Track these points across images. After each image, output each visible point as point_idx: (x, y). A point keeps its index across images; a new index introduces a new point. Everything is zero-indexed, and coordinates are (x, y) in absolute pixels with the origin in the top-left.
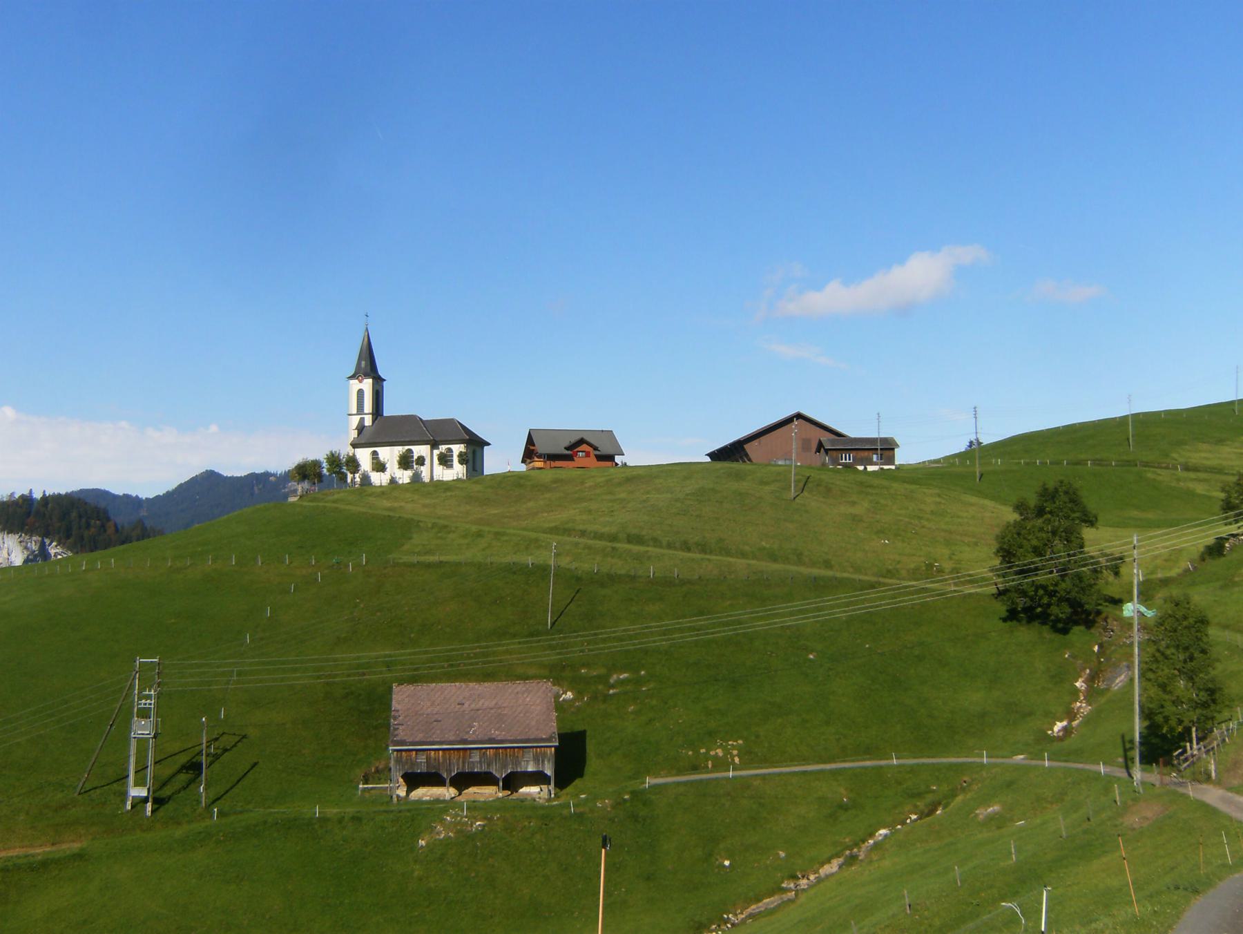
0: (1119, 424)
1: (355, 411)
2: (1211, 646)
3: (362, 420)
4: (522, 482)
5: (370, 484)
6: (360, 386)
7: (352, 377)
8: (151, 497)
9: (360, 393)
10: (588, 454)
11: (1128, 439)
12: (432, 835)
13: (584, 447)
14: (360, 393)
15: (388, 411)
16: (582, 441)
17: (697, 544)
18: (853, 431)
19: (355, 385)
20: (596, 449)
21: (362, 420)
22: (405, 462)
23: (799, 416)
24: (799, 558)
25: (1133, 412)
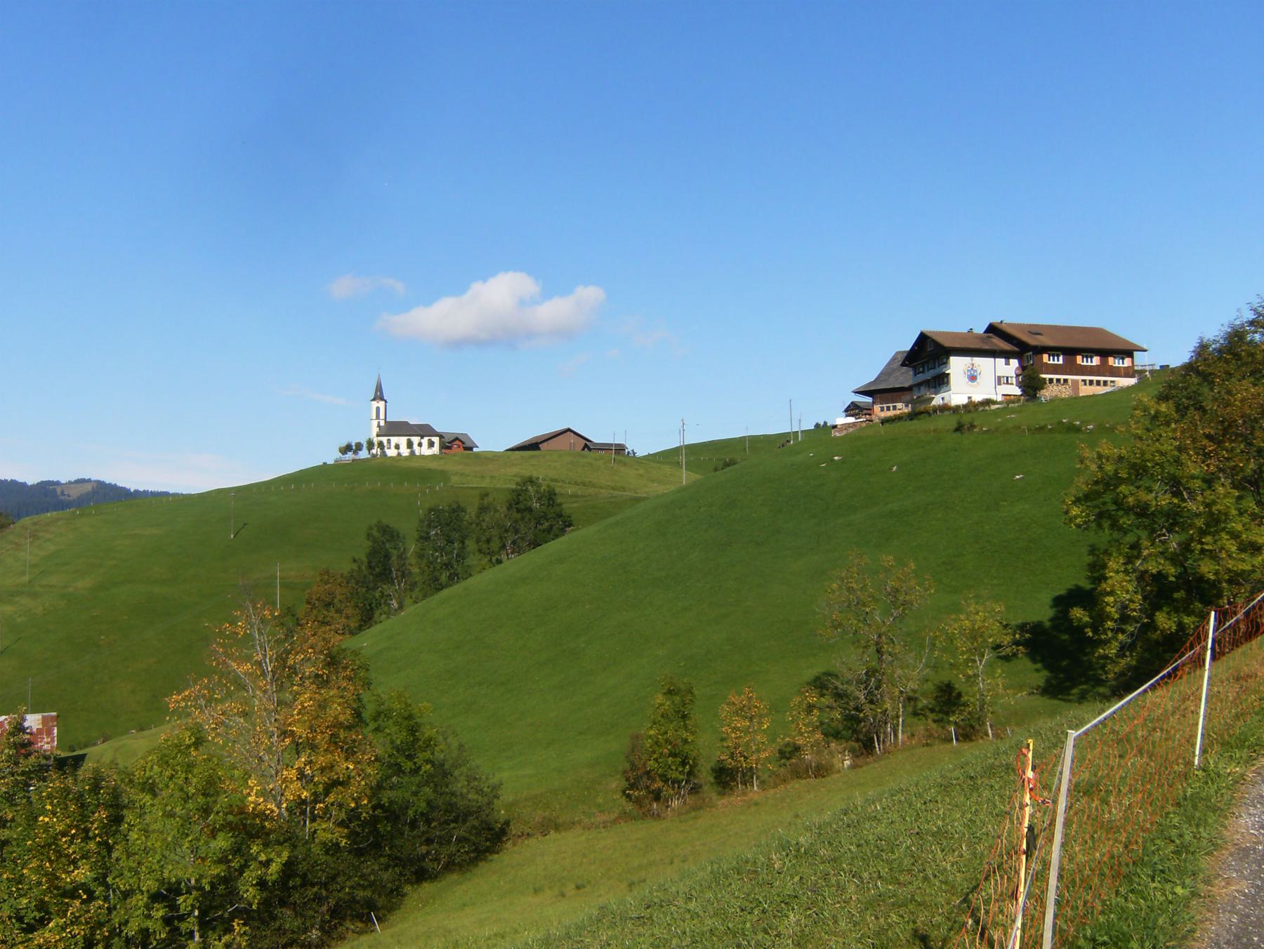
0: (742, 440)
1: (374, 417)
2: (570, 517)
3: (379, 423)
4: (966, 419)
5: (386, 456)
6: (378, 405)
7: (373, 400)
8: (30, 483)
9: (378, 409)
10: (459, 447)
11: (745, 449)
12: (477, 553)
13: (457, 442)
14: (378, 409)
15: (388, 420)
16: (457, 439)
17: (581, 483)
18: (597, 438)
19: (375, 404)
20: (463, 443)
21: (379, 423)
22: (410, 445)
23: (569, 430)
24: (624, 489)
25: (692, 439)
